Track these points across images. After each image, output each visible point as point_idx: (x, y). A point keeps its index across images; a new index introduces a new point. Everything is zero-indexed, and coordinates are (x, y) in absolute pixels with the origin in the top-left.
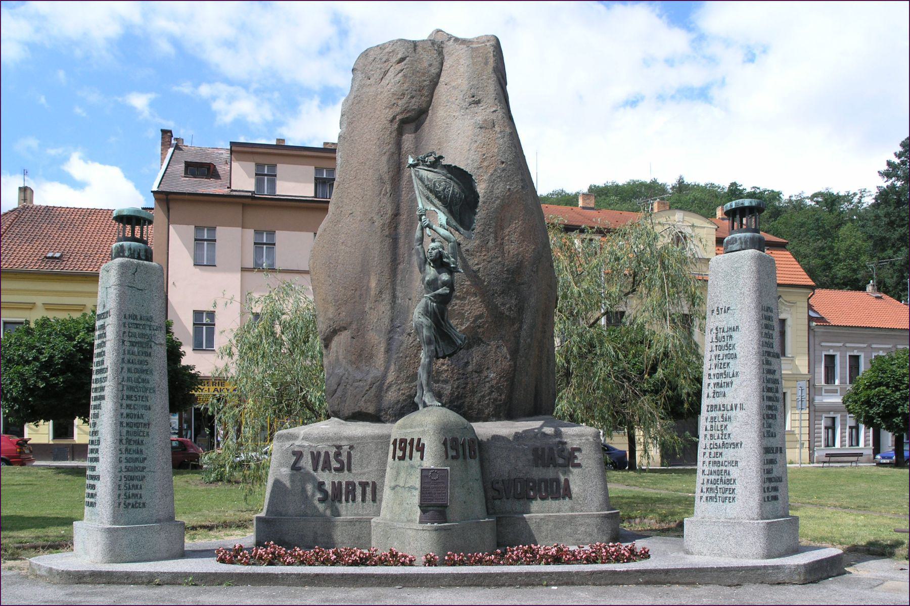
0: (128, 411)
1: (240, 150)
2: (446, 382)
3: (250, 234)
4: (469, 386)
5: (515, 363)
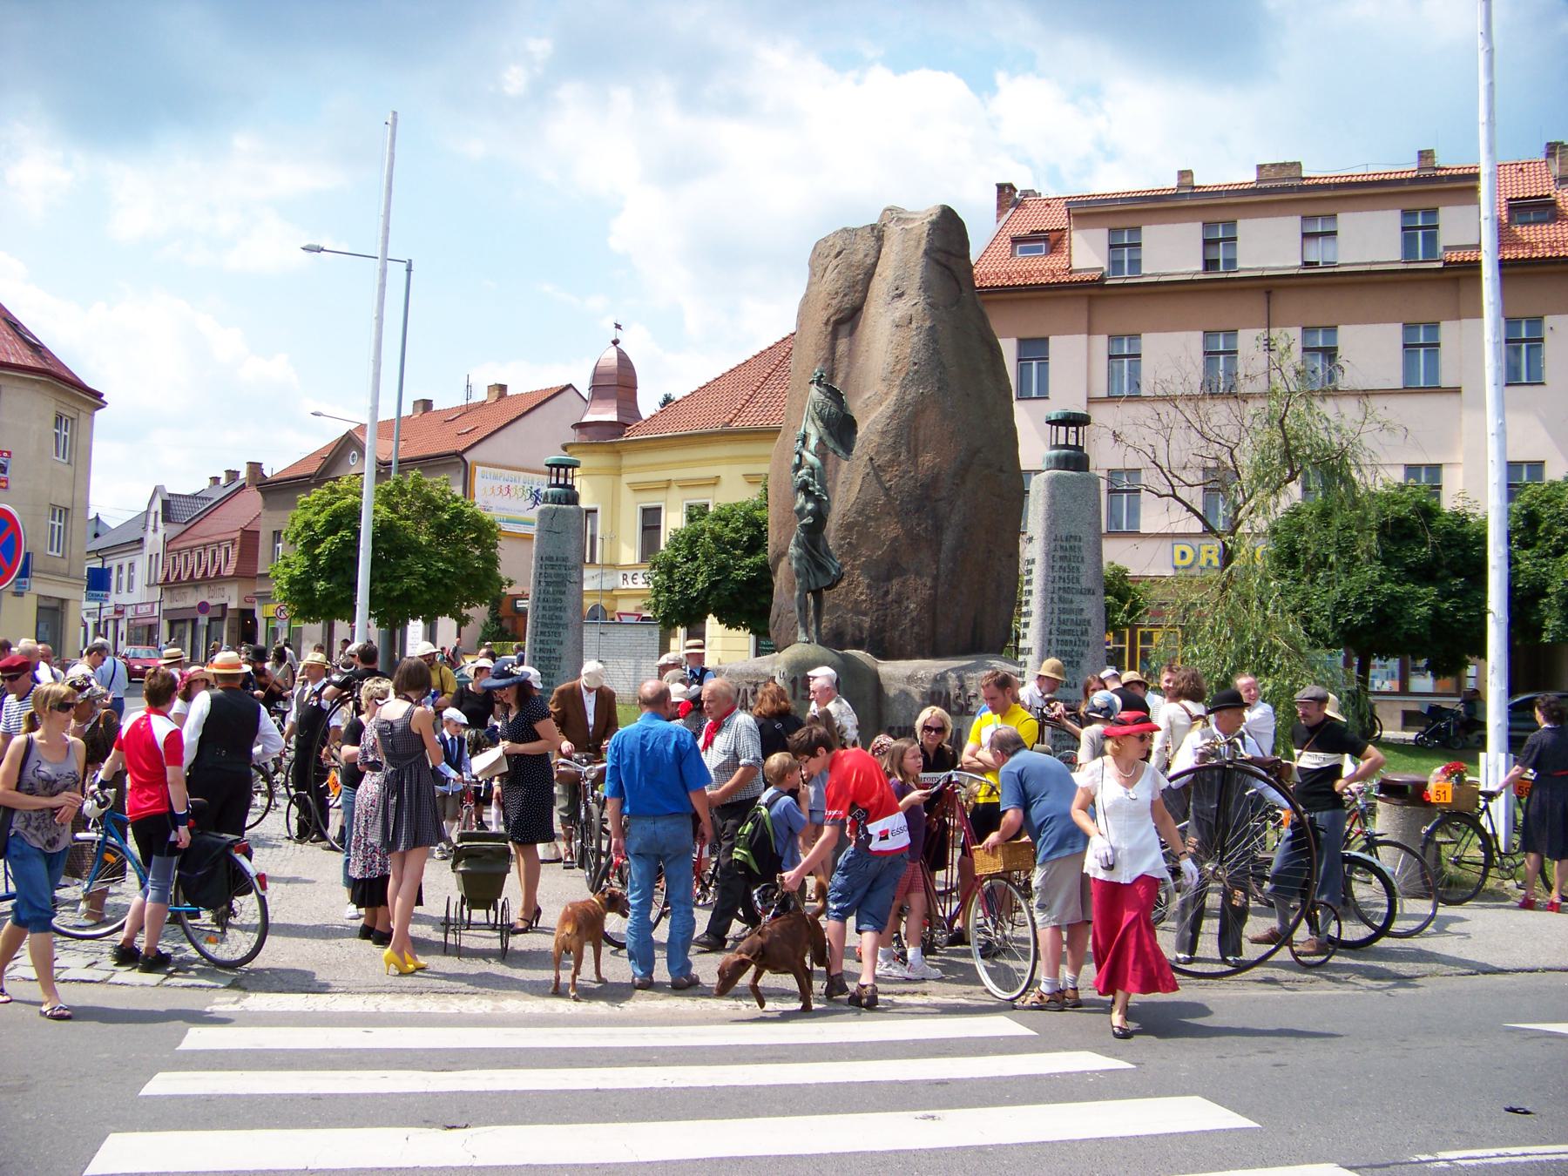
0: (542, 646)
1: (1086, 211)
2: (865, 614)
3: (1101, 342)
4: (889, 618)
5: (936, 591)
